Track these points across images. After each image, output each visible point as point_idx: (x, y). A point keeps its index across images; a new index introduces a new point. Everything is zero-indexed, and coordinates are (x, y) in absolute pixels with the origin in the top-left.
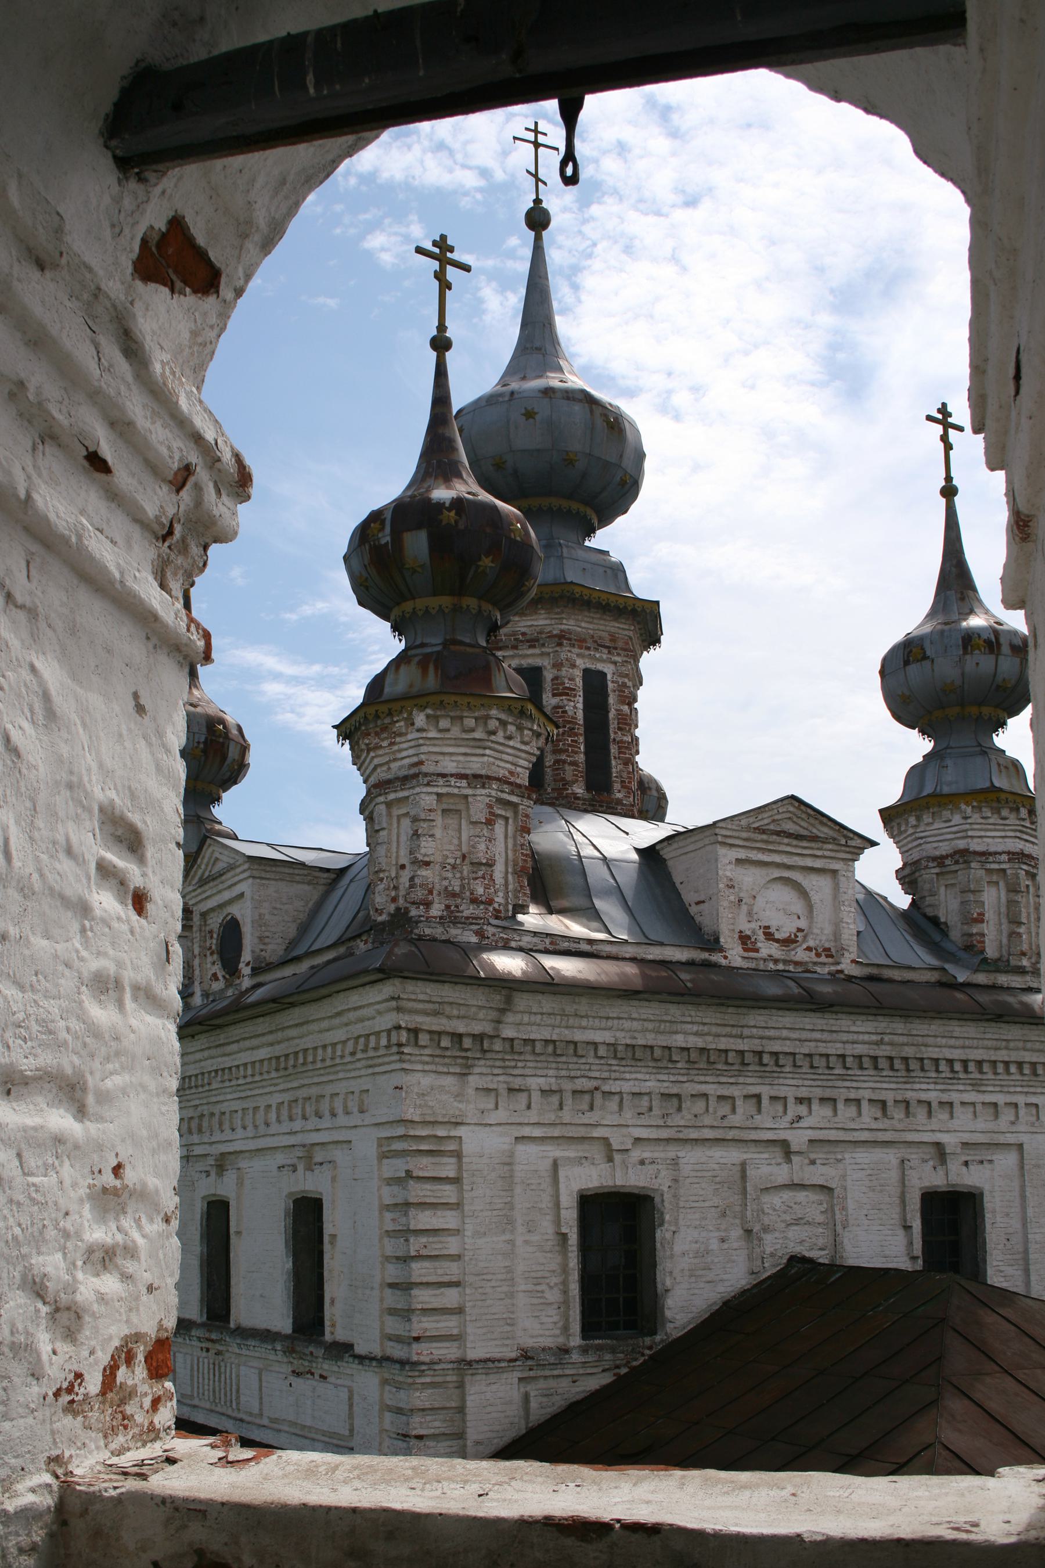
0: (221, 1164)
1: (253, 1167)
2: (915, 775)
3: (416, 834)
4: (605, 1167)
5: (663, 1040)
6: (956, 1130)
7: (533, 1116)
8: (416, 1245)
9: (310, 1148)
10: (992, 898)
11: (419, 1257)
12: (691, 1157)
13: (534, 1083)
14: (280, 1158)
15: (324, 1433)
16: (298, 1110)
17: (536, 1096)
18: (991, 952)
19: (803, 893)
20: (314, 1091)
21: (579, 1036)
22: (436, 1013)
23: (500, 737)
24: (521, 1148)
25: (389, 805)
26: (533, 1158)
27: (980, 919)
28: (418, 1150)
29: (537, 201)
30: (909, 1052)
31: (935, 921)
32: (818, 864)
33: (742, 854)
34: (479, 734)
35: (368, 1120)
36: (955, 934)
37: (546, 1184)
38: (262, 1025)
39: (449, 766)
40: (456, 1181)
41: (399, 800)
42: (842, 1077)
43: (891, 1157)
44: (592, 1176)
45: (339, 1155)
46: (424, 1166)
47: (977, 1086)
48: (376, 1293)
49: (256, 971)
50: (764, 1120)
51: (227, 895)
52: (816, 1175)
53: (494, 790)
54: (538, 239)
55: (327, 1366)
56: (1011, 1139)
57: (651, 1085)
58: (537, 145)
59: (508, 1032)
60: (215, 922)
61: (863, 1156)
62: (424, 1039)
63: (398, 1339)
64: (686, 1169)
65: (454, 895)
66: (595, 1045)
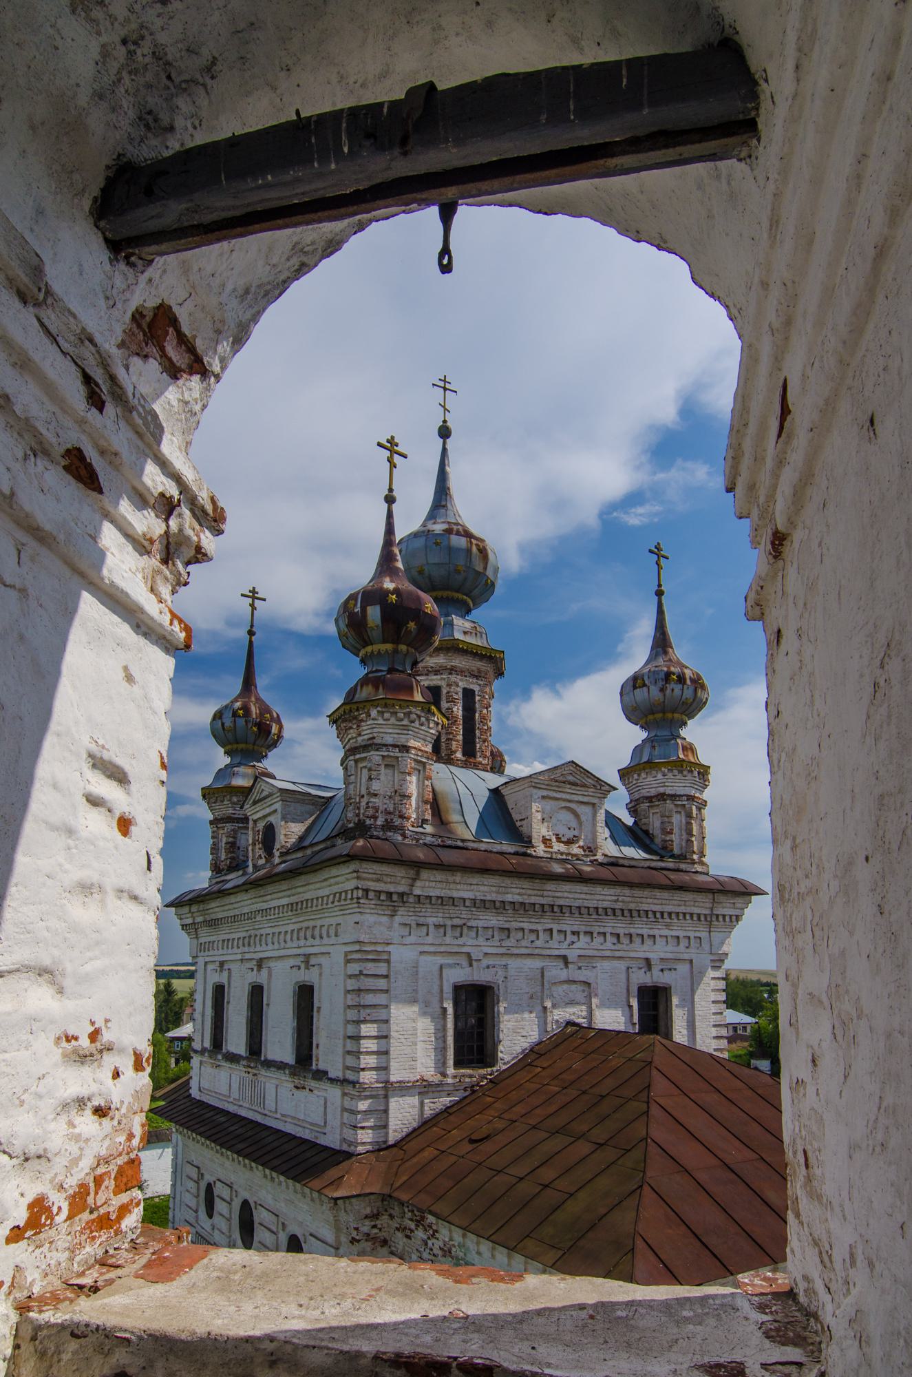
0: (260, 963)
2: (637, 750)
3: (370, 779)
4: (468, 970)
5: (500, 898)
7: (430, 939)
8: (364, 1013)
10: (677, 820)
12: (513, 963)
13: (431, 921)
14: (292, 962)
15: (311, 1124)
17: (431, 928)
18: (676, 851)
20: (311, 924)
21: (455, 894)
22: (378, 880)
23: (417, 724)
24: (423, 958)
25: (356, 761)
26: (430, 964)
27: (671, 833)
28: (369, 960)
29: (445, 421)
30: (632, 906)
31: (646, 832)
32: (585, 799)
33: (545, 793)
34: (405, 722)
35: (340, 940)
36: (658, 840)
38: (284, 885)
39: (389, 740)
40: (387, 977)
42: (596, 920)
43: (622, 965)
46: (371, 968)
47: (668, 926)
49: (282, 854)
51: (268, 810)
55: (313, 1084)
56: (686, 957)
58: (445, 389)
59: (417, 892)
60: (261, 825)
61: (607, 964)
62: (371, 895)
64: (512, 972)
65: (390, 813)
66: (464, 900)
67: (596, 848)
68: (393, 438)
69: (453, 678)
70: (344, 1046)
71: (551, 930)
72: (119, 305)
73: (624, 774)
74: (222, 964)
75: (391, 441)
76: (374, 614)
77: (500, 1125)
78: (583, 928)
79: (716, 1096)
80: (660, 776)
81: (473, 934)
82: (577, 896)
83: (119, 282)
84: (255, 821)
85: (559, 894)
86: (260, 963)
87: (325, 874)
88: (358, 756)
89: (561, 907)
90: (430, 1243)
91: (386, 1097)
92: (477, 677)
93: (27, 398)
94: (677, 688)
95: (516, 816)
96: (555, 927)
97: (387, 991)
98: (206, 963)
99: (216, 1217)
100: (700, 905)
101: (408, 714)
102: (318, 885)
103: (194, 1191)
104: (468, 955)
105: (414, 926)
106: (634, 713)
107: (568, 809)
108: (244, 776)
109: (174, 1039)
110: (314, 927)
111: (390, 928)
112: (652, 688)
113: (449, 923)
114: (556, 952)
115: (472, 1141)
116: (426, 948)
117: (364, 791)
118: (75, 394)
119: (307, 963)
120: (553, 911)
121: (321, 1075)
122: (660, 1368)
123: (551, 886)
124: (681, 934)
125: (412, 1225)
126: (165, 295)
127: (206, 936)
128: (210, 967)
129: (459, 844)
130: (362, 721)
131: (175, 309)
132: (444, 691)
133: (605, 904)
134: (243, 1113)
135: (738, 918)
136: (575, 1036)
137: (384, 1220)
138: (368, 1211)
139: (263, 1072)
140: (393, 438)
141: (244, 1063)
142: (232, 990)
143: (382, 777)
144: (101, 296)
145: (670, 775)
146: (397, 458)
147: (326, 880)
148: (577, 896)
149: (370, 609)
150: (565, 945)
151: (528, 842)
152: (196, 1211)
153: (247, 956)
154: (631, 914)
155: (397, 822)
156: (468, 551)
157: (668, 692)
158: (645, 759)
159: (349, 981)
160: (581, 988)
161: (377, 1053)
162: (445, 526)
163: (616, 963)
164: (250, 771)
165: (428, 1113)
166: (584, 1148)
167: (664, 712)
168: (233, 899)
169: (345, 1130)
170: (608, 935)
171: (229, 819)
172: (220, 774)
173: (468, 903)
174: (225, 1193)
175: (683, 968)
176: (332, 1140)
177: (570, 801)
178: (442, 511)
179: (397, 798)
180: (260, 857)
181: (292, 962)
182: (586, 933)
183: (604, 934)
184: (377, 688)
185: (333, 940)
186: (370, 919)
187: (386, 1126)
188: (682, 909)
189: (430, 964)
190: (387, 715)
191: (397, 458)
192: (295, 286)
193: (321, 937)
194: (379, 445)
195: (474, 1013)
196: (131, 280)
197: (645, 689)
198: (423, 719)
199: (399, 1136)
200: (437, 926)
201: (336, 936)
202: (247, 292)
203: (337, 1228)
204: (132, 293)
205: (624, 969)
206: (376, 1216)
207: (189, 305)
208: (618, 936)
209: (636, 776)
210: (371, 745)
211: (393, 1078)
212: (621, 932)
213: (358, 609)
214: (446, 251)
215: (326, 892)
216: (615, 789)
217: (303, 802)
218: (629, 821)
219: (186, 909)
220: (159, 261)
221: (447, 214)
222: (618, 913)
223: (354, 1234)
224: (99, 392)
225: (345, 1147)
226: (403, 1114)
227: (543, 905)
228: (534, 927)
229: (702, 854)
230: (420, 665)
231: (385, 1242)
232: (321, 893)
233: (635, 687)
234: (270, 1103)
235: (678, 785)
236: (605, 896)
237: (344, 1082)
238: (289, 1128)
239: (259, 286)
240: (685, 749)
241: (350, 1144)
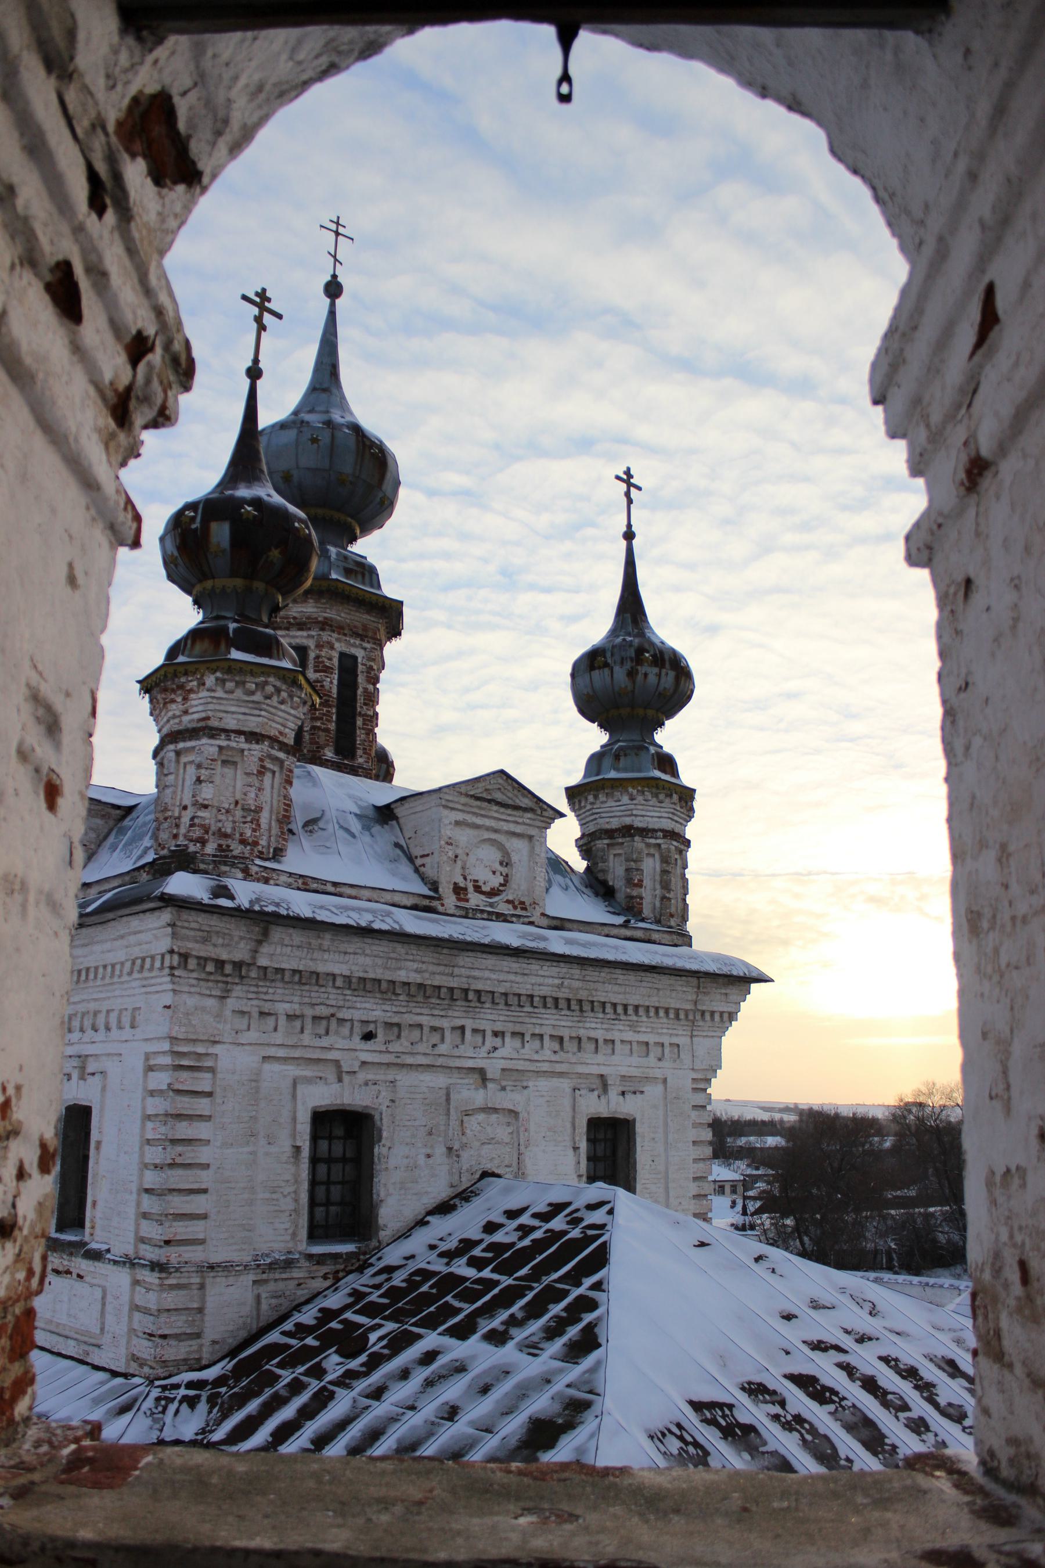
2: (596, 761)
3: (199, 781)
4: (336, 1086)
5: (388, 976)
6: (619, 1064)
7: (279, 1038)
9: (83, 1058)
10: (650, 866)
12: (405, 1079)
17: (282, 1021)
20: (92, 1006)
21: (321, 968)
24: (267, 1067)
25: (178, 753)
27: (639, 884)
29: (334, 276)
30: (583, 995)
31: (604, 883)
32: (518, 829)
33: (460, 816)
39: (231, 723)
47: (633, 1027)
50: (466, 1050)
53: (265, 746)
54: (333, 305)
56: (658, 1073)
58: (337, 234)
59: (263, 962)
61: (543, 1084)
62: (192, 963)
65: (226, 836)
66: (334, 976)
68: (264, 290)
69: (326, 636)
70: (138, 1204)
71: (462, 1028)
72: (119, 87)
73: (573, 793)
75: (263, 295)
76: (221, 533)
78: (510, 1027)
80: (625, 799)
82: (502, 977)
83: (124, 59)
85: (476, 973)
88: (181, 745)
89: (478, 992)
92: (362, 637)
93: (31, 195)
96: (469, 1024)
100: (680, 996)
105: (255, 1015)
106: (591, 705)
107: (493, 842)
110: (96, 1013)
112: (617, 669)
114: (470, 1064)
116: (272, 1052)
117: (187, 800)
118: (79, 190)
119: (83, 1068)
120: (467, 1000)
122: (869, 1556)
123: (465, 960)
124: (651, 1039)
126: (167, 81)
130: (191, 691)
131: (176, 100)
132: (312, 655)
133: (545, 991)
135: (732, 1016)
140: (264, 290)
143: (217, 779)
144: (102, 73)
145: (640, 798)
146: (267, 318)
147: (122, 937)
148: (502, 977)
149: (214, 526)
150: (483, 1052)
154: (580, 1006)
157: (640, 677)
159: (150, 1100)
160: (503, 1119)
163: (555, 1082)
169: (135, 1341)
170: (546, 1038)
173: (339, 982)
177: (496, 831)
182: (514, 1034)
183: (541, 1036)
184: (217, 645)
185: (127, 1033)
188: (653, 1001)
190: (230, 685)
191: (267, 318)
192: (318, 91)
193: (108, 1029)
194: (245, 298)
196: (137, 59)
197: (607, 671)
198: (284, 694)
201: (133, 1027)
202: (260, 88)
204: (136, 73)
205: (568, 1090)
207: (192, 96)
208: (561, 1039)
209: (591, 798)
210: (204, 730)
212: (566, 1033)
214: (566, 77)
215: (120, 956)
216: (562, 815)
218: (579, 864)
220: (172, 40)
221: (566, 40)
222: (562, 1004)
224: (105, 193)
227: (451, 990)
228: (437, 1023)
230: (282, 613)
232: (110, 958)
235: (653, 814)
239: (275, 85)
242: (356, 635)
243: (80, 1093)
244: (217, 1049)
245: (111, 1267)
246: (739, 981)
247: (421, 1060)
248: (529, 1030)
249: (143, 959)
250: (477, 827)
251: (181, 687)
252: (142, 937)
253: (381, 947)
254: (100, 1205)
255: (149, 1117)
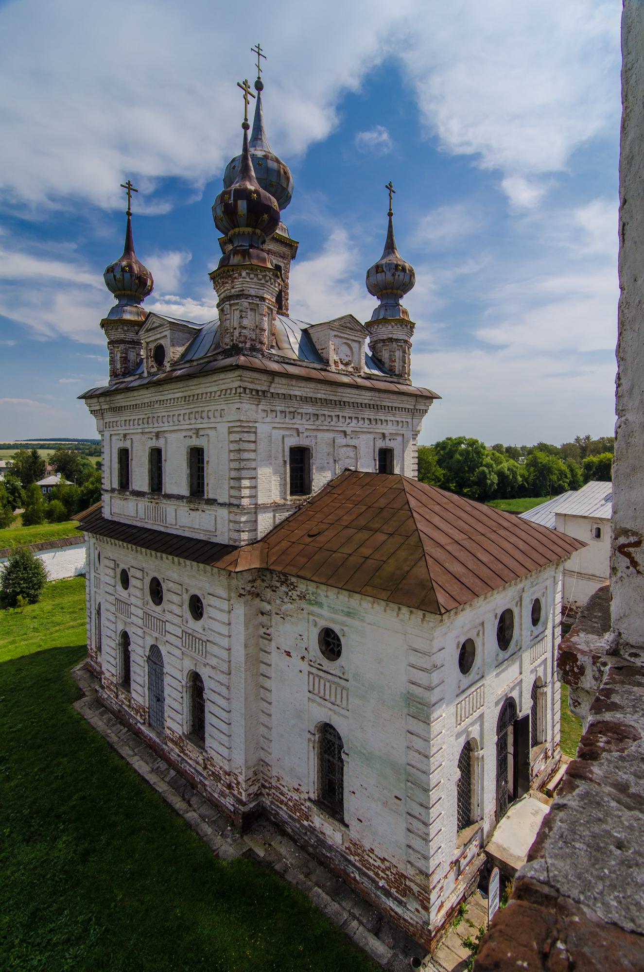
0: (158, 435)
1: (171, 437)
2: (377, 311)
3: (241, 317)
4: (297, 438)
5: (314, 396)
6: (389, 429)
7: (277, 420)
8: (243, 464)
9: (198, 430)
10: (398, 354)
11: (243, 469)
12: (320, 435)
14: (185, 434)
15: (203, 530)
16: (192, 416)
17: (278, 413)
18: (397, 372)
19: (351, 348)
20: (200, 409)
21: (292, 393)
22: (252, 382)
23: (269, 283)
25: (231, 305)
26: (277, 434)
27: (395, 361)
28: (243, 431)
29: (259, 78)
30: (379, 403)
31: (380, 361)
32: (356, 339)
33: (336, 333)
34: (263, 282)
35: (225, 419)
36: (387, 366)
37: (281, 443)
38: (180, 385)
39: (253, 293)
40: (255, 442)
41: (234, 304)
42: (361, 411)
43: (371, 436)
44: (293, 441)
45: (211, 433)
46: (246, 437)
47: (394, 415)
48: (227, 481)
49: (172, 365)
50: (340, 424)
51: (159, 336)
52: (353, 442)
55: (205, 507)
56: (401, 432)
57: (310, 411)
58: (259, 54)
59: (272, 390)
60: (152, 346)
62: (248, 391)
63: (235, 497)
65: (253, 340)
66: (296, 396)
67: (361, 368)
74: (125, 435)
76: (242, 206)
77: (325, 526)
78: (354, 415)
79: (438, 506)
80: (390, 327)
81: (300, 417)
84: (147, 343)
86: (158, 435)
87: (215, 377)
90: (290, 593)
91: (256, 513)
94: (402, 274)
95: (318, 347)
97: (255, 451)
98: (111, 435)
99: (131, 589)
100: (409, 403)
101: (264, 276)
102: (208, 385)
103: (112, 574)
104: (297, 430)
106: (375, 289)
108: (131, 313)
109: (42, 486)
111: (257, 412)
113: (287, 410)
115: (310, 536)
117: (236, 325)
119: (197, 434)
121: (212, 502)
123: (340, 390)
124: (399, 419)
125: (278, 584)
127: (109, 417)
128: (114, 438)
129: (292, 362)
130: (235, 278)
133: (366, 401)
134: (149, 526)
135: (426, 411)
136: (350, 476)
137: (259, 582)
138: (250, 578)
139: (164, 501)
141: (149, 496)
142: (134, 452)
149: (239, 202)
151: (327, 363)
152: (114, 586)
153: (147, 430)
154: (376, 407)
155: (258, 346)
156: (279, 172)
157: (396, 277)
158: (381, 317)
161: (250, 488)
162: (264, 153)
164: (134, 309)
165: (278, 521)
166: (382, 537)
167: (392, 289)
168: (135, 393)
169: (231, 533)
171: (122, 341)
172: (114, 310)
174: (139, 574)
175: (399, 439)
176: (222, 538)
178: (259, 142)
179: (258, 331)
180: (152, 366)
181: (185, 434)
184: (244, 258)
186: (246, 406)
187: (255, 530)
189: (277, 434)
190: (252, 276)
195: (299, 461)
199: (263, 535)
200: (281, 412)
203: (229, 589)
206: (253, 581)
208: (370, 420)
210: (241, 295)
211: (259, 502)
213: (231, 201)
215: (215, 389)
217: (182, 331)
219: (95, 400)
223: (242, 592)
225: (231, 543)
226: (265, 522)
228: (330, 414)
229: (409, 375)
231: (258, 595)
233: (377, 272)
234: (171, 519)
235: (399, 334)
236: (366, 397)
237: (230, 505)
238: (187, 534)
240: (403, 312)
241: (235, 541)
242: (281, 257)
243: (195, 442)
244: (257, 425)
245: (219, 507)
246: (429, 397)
247: (325, 428)
248: (360, 416)
249: (226, 390)
250: (341, 337)
251: (230, 276)
252: (226, 381)
253: (312, 385)
254: (210, 485)
255: (231, 451)
